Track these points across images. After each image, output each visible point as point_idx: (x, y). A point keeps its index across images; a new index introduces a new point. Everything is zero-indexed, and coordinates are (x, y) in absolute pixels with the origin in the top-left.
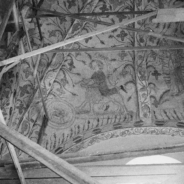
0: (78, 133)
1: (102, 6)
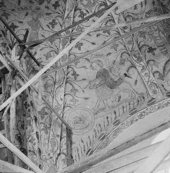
1: (79, 14)
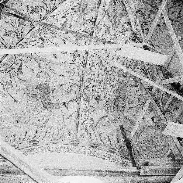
0: (14, 141)
1: (63, 22)
